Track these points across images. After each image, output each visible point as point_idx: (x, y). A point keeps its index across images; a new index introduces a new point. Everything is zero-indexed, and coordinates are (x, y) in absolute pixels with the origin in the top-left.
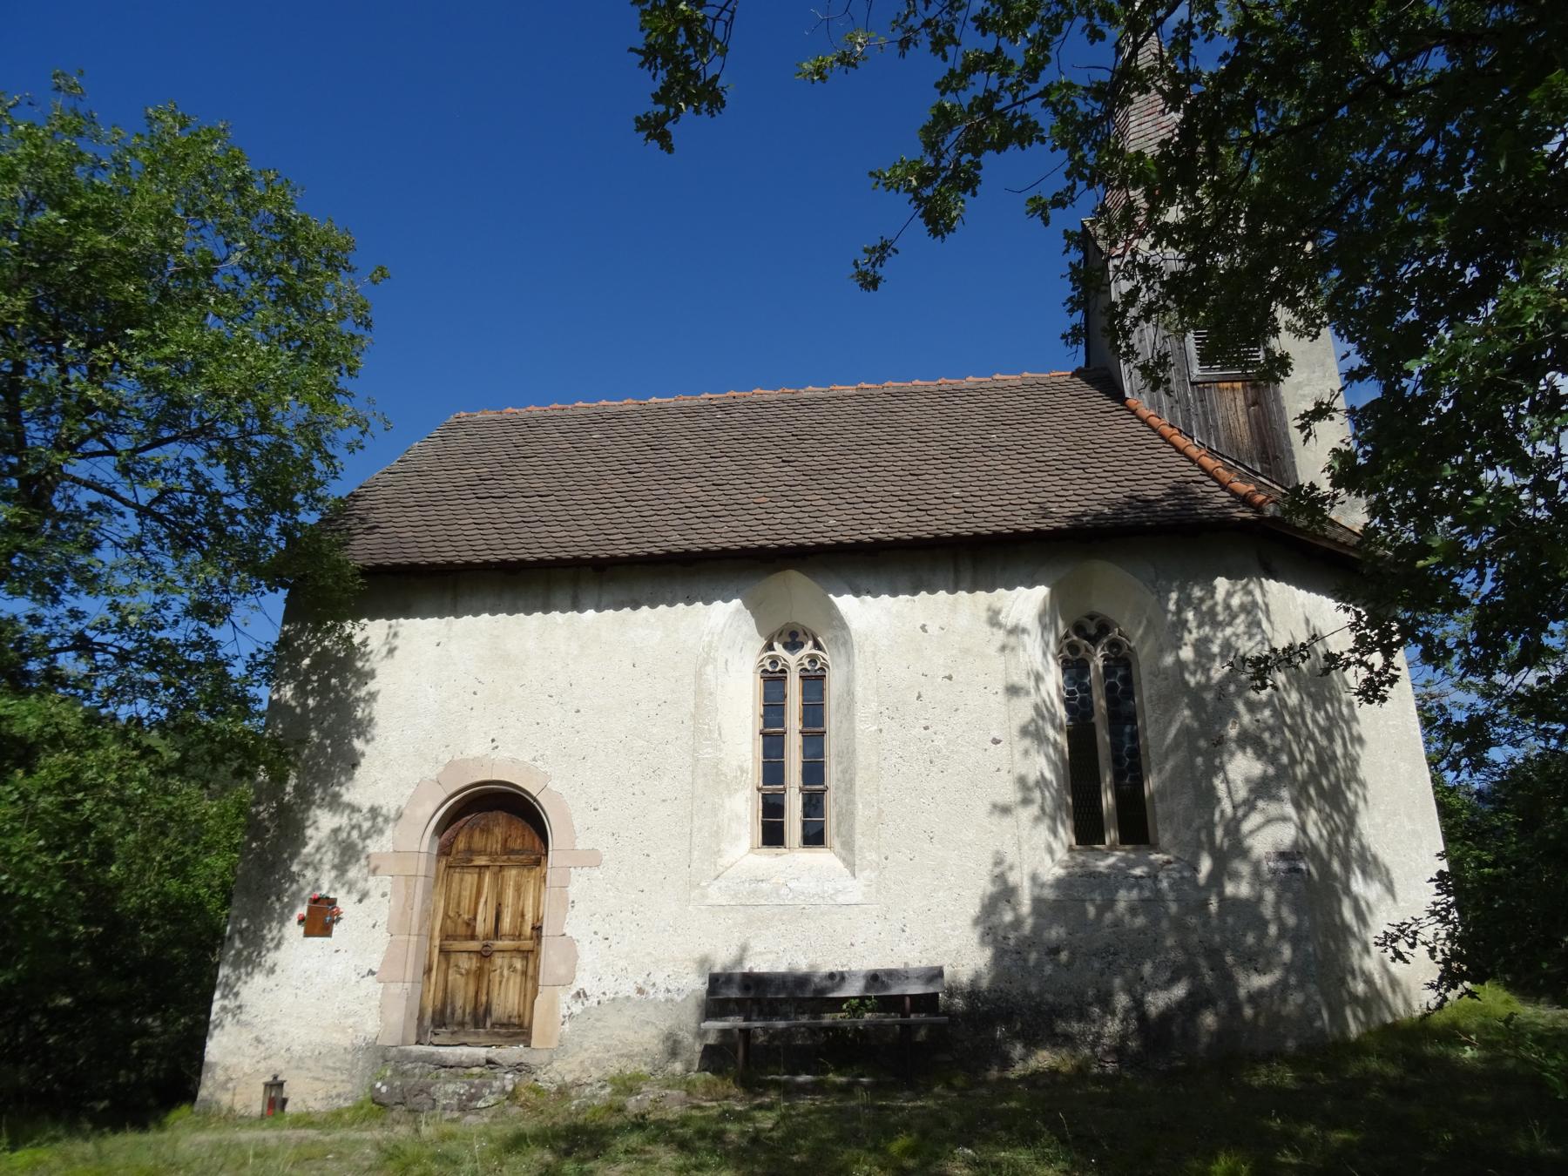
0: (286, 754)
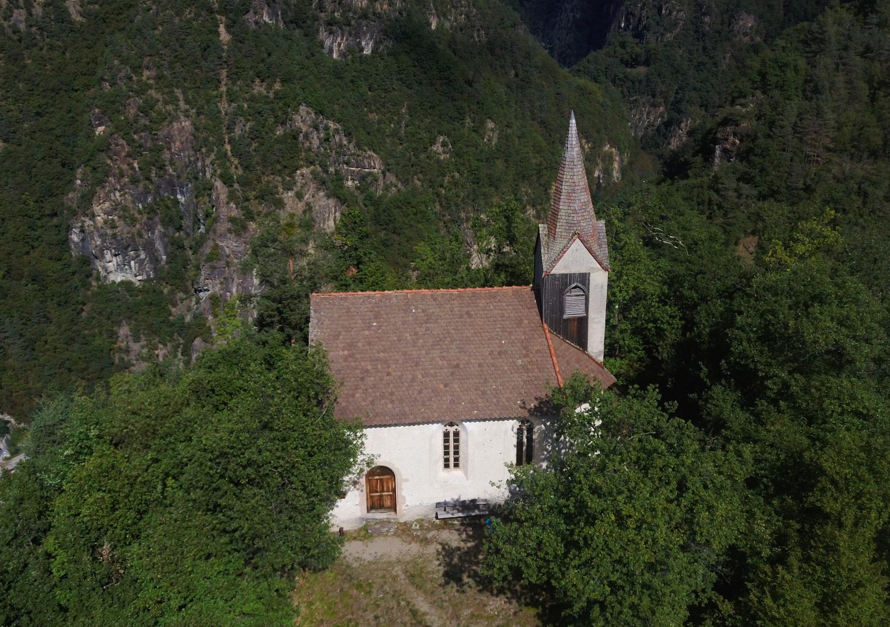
0: (457, 221)
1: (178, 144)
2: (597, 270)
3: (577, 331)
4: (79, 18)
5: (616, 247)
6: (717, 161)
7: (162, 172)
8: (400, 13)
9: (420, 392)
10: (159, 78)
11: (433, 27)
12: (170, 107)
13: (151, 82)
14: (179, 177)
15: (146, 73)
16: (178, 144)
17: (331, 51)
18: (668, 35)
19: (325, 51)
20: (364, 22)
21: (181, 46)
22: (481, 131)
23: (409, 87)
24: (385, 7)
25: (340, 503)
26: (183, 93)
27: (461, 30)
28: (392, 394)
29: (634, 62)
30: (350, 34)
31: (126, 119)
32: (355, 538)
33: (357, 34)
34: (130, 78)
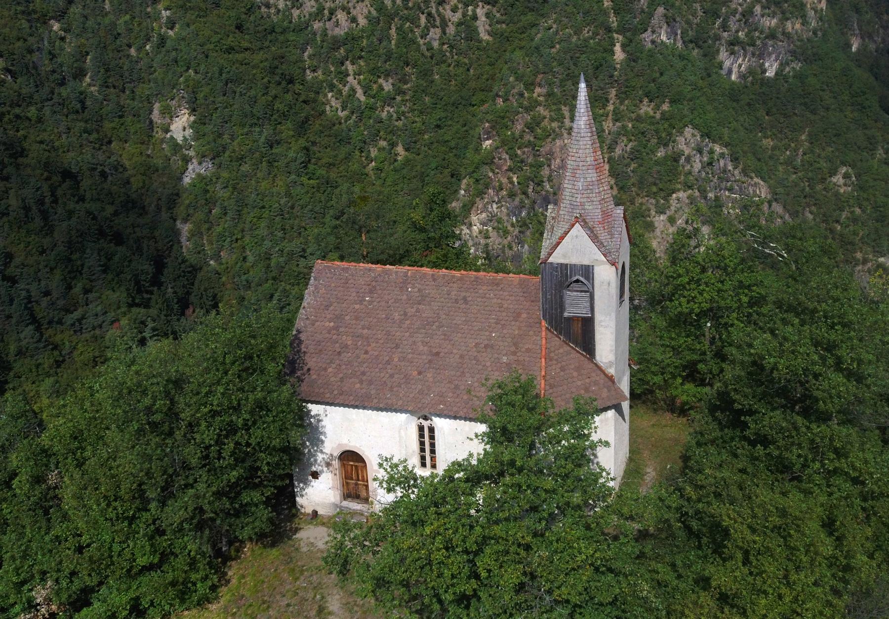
1: (558, 160)
2: (602, 263)
3: (582, 334)
7: (539, 188)
8: (815, 33)
9: (392, 376)
10: (549, 95)
12: (555, 125)
13: (541, 99)
15: (538, 90)
16: (558, 160)
17: (730, 72)
19: (724, 72)
20: (770, 43)
21: (575, 64)
23: (814, 112)
24: (798, 26)
25: (315, 483)
28: (363, 373)
30: (753, 55)
31: (513, 134)
32: (323, 524)
34: (521, 95)
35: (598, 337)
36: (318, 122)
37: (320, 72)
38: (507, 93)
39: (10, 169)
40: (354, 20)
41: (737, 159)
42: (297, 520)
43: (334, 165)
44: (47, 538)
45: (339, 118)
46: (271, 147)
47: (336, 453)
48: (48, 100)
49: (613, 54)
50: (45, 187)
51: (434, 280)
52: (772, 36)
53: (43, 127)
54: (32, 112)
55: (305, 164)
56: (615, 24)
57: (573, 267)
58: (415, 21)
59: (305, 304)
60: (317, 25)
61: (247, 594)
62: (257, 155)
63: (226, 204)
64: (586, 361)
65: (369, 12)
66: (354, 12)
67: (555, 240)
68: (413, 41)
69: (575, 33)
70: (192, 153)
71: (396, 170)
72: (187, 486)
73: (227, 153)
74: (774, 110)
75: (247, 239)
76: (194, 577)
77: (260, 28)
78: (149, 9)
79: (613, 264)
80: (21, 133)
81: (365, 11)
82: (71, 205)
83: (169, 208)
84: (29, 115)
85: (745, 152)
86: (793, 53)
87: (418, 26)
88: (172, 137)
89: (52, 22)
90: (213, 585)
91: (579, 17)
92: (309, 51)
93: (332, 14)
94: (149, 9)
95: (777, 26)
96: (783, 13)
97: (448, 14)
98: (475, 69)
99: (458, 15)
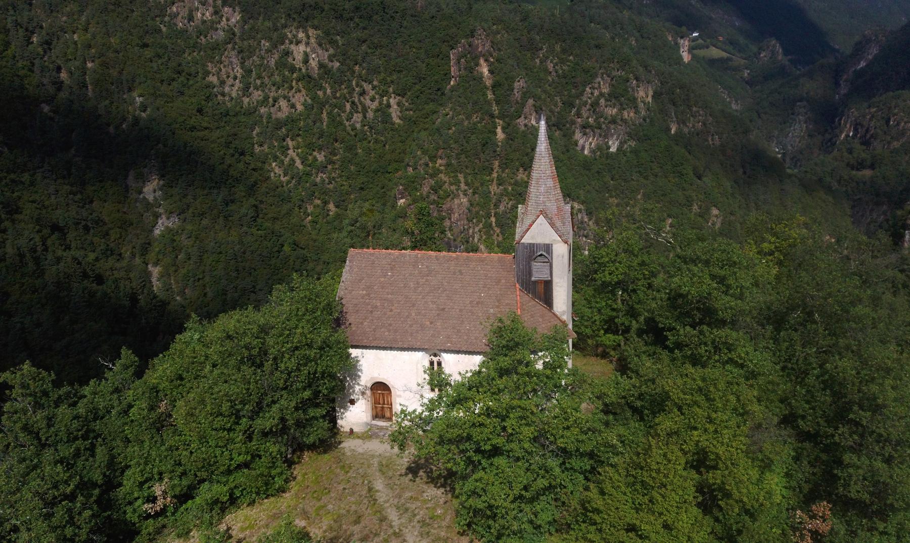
1: (456, 215)
2: (558, 242)
3: (543, 292)
4: (398, 121)
5: (578, 227)
6: (906, 245)
7: (443, 236)
8: (644, 120)
9: (411, 326)
10: (448, 165)
11: (673, 132)
12: (453, 188)
13: (442, 168)
14: (455, 240)
15: (439, 161)
16: (456, 215)
17: (583, 148)
18: (895, 143)
19: (579, 148)
20: (612, 126)
21: (467, 142)
22: (706, 216)
23: (646, 178)
24: (632, 114)
25: (352, 408)
26: (465, 177)
27: (698, 134)
28: (390, 325)
29: (860, 166)
30: (600, 135)
31: (421, 194)
32: (359, 437)
33: (606, 136)
34: (427, 165)
35: (555, 293)
36: (266, 185)
37: (266, 147)
38: (416, 163)
39: (7, 224)
40: (293, 106)
41: (590, 213)
42: (338, 436)
43: (277, 219)
44: (163, 448)
45: (281, 182)
46: (227, 205)
47: (369, 385)
48: (39, 168)
49: (496, 134)
50: (37, 239)
51: (438, 260)
52: (613, 121)
53: (35, 189)
54: (26, 177)
55: (254, 219)
56: (497, 112)
57: (538, 246)
58: (342, 108)
59: (343, 279)
60: (263, 110)
61: (312, 485)
62: (215, 211)
63: (190, 250)
64: (547, 311)
65: (305, 100)
66: (293, 100)
67: (524, 228)
68: (341, 123)
69: (467, 119)
70: (161, 210)
71: (328, 223)
72: (274, 402)
73: (191, 210)
74: (617, 177)
75: (207, 279)
76: (273, 472)
77: (217, 112)
78: (125, 96)
79: (566, 243)
80: (16, 194)
81: (302, 99)
82: (59, 253)
83: (142, 255)
84: (23, 180)
85: (596, 208)
86: (629, 134)
87: (344, 112)
88: (144, 198)
89: (43, 105)
90: (287, 478)
91: (469, 107)
92: (257, 130)
93: (275, 102)
94: (125, 96)
95: (617, 114)
96: (621, 105)
97: (368, 102)
98: (390, 145)
99: (376, 103)
